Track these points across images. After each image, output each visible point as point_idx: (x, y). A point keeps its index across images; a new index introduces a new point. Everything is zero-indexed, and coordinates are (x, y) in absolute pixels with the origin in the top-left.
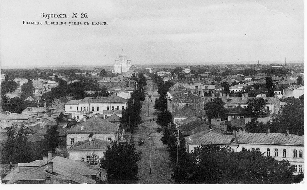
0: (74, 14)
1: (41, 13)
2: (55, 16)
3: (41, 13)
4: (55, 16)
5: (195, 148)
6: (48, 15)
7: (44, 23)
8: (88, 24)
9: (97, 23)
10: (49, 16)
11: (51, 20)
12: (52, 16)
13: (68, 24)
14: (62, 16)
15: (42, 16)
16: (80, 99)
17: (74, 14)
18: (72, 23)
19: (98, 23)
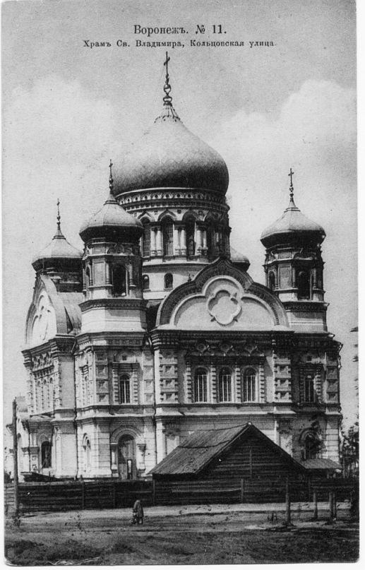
0: (198, 26)
1: (136, 26)
2: (163, 30)
3: (136, 26)
4: (163, 30)
5: (273, 518)
6: (149, 29)
7: (113, 43)
8: (109, 45)
9: (202, 44)
10: (151, 31)
11: (156, 37)
12: (156, 31)
13: (247, 45)
14: (175, 31)
15: (138, 31)
16: (176, 474)
17: (198, 26)
18: (255, 43)
19: (204, 43)
